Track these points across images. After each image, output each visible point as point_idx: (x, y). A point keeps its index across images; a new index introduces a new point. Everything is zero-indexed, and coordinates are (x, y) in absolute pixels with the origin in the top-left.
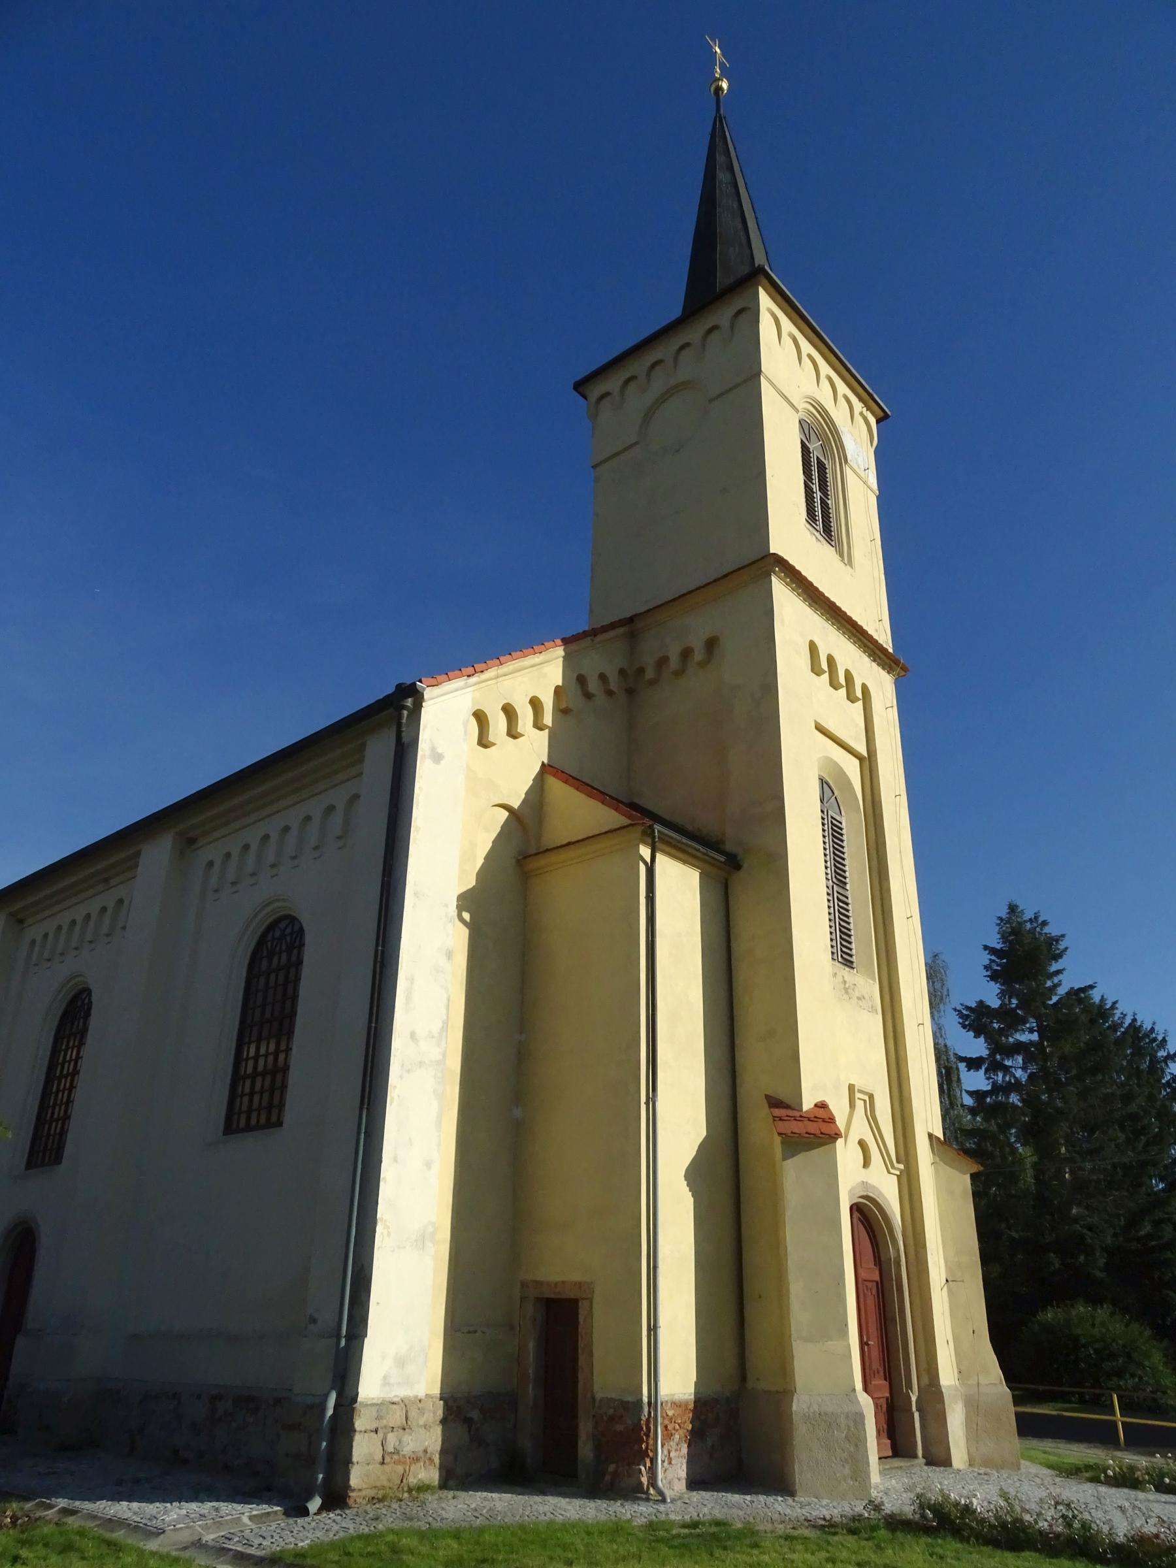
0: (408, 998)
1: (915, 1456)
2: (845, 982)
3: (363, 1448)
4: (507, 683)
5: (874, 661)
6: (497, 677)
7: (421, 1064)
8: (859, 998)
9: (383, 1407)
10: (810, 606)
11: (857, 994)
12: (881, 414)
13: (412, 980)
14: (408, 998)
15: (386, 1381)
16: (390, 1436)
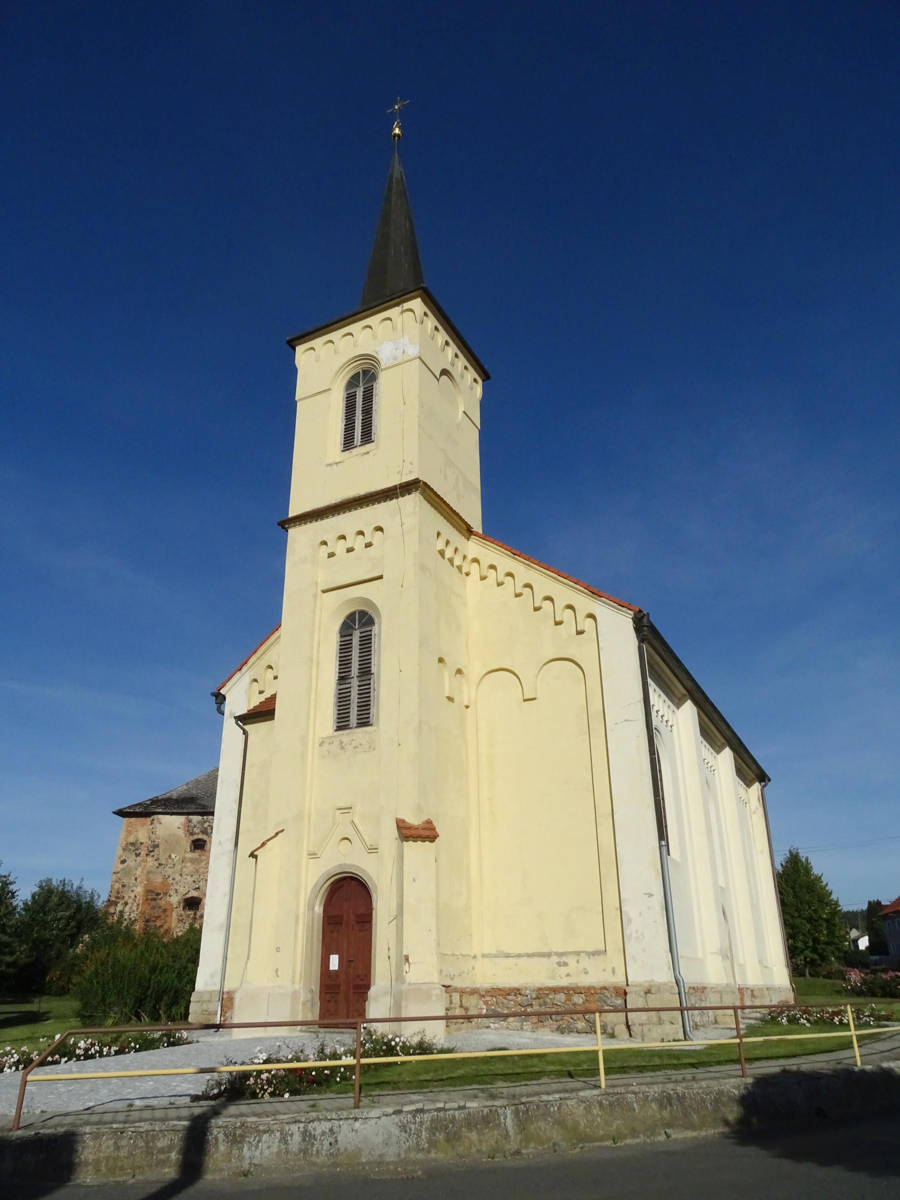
1: (595, 1032)
2: (342, 743)
4: (267, 656)
5: (391, 500)
6: (259, 658)
8: (355, 748)
10: (322, 519)
11: (354, 744)
12: (419, 292)
15: (206, 983)
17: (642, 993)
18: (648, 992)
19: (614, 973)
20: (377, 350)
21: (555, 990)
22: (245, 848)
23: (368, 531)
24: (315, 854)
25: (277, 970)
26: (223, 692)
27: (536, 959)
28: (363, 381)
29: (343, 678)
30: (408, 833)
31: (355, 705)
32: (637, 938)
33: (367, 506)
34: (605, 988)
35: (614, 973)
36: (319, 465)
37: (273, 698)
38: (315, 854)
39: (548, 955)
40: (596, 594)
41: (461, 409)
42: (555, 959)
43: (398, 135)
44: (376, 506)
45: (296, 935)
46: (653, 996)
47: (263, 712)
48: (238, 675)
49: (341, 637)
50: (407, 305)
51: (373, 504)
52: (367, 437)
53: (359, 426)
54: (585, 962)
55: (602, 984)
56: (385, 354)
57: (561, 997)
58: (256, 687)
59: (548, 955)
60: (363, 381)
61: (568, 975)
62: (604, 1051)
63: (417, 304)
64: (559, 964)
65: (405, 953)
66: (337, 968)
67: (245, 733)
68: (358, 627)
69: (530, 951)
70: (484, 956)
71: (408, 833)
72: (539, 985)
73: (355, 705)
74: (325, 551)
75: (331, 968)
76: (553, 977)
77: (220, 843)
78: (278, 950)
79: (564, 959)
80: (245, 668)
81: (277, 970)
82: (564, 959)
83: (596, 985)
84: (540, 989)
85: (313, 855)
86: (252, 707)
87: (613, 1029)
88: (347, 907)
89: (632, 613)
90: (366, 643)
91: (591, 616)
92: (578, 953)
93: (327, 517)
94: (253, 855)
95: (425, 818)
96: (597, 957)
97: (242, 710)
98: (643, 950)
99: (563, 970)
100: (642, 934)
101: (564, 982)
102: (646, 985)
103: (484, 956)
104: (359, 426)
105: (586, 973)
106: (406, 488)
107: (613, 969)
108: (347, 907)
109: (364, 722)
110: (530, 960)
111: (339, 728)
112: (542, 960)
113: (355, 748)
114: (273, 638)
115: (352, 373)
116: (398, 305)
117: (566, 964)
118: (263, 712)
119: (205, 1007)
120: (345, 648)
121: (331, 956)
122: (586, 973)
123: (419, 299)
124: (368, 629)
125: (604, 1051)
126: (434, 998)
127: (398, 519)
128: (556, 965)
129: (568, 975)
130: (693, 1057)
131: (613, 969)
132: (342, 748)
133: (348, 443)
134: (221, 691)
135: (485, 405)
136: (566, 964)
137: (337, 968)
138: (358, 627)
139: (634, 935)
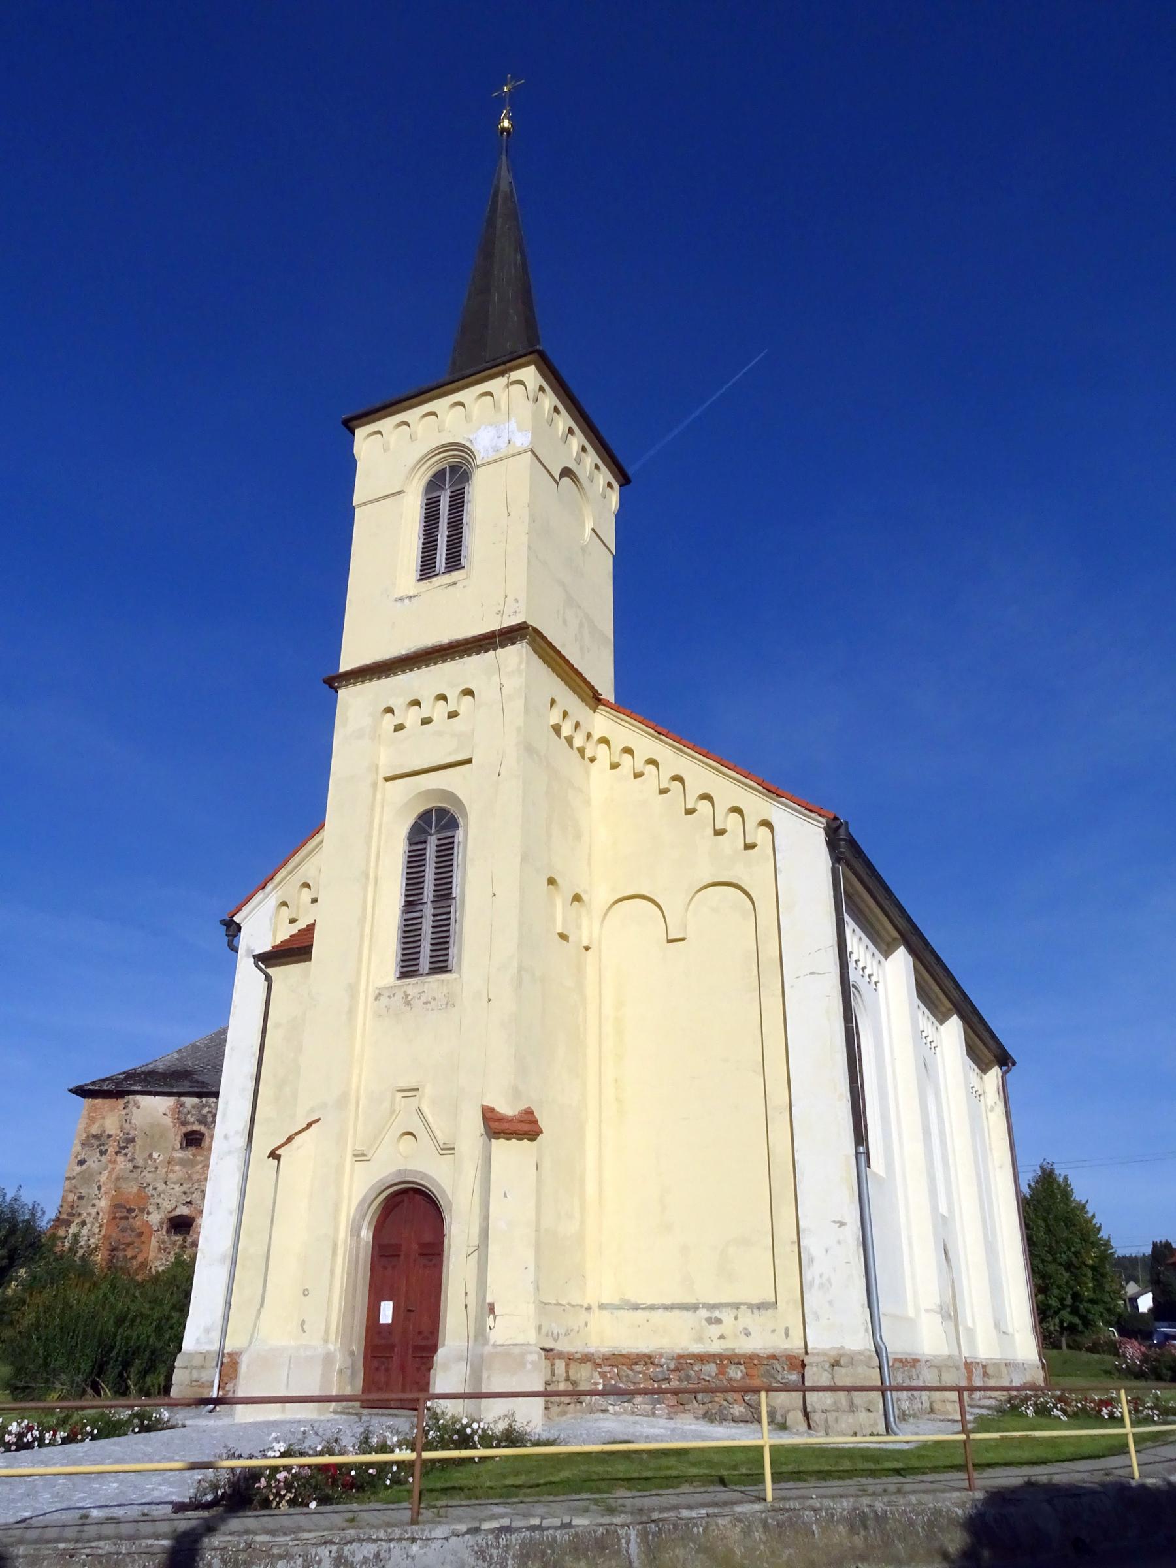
0: (224, 1115)
2: (407, 996)
3: (177, 1376)
4: (303, 869)
5: (487, 651)
6: (291, 872)
7: (230, 1152)
8: (426, 1003)
9: (191, 1355)
10: (387, 677)
11: (424, 999)
13: (227, 1103)
14: (224, 1115)
16: (194, 1372)
17: (827, 1366)
18: (836, 1364)
19: (787, 1335)
20: (471, 437)
21: (702, 1358)
22: (263, 1144)
24: (364, 1155)
25: (303, 1322)
26: (237, 919)
27: (677, 1312)
29: (411, 903)
30: (498, 1127)
31: (427, 941)
32: (821, 1286)
33: (452, 659)
34: (774, 1357)
35: (787, 1335)
36: (384, 596)
37: (311, 928)
38: (364, 1155)
39: (694, 1308)
40: (773, 791)
41: (589, 525)
42: (703, 1313)
43: (507, 130)
44: (465, 659)
46: (844, 1371)
47: (295, 950)
48: (260, 895)
49: (410, 844)
50: (515, 375)
51: (461, 657)
52: (455, 561)
53: (443, 543)
54: (747, 1319)
55: (770, 1351)
56: (483, 443)
57: (712, 1368)
59: (694, 1308)
61: (722, 1337)
62: (773, 1448)
63: (529, 374)
64: (709, 1321)
65: (489, 1300)
66: (390, 1321)
67: (268, 978)
68: (435, 834)
69: (668, 1302)
70: (602, 1307)
71: (498, 1127)
72: (678, 1351)
73: (427, 941)
74: (389, 721)
75: (382, 1321)
76: (700, 1340)
77: (226, 1137)
78: (306, 1293)
79: (717, 1314)
80: (270, 887)
81: (303, 1322)
82: (717, 1314)
83: (761, 1352)
84: (680, 1357)
85: (360, 1156)
87: (784, 1417)
88: (407, 1233)
89: (823, 820)
90: (446, 853)
91: (766, 824)
92: (736, 1306)
93: (395, 674)
95: (523, 1107)
96: (763, 1312)
97: (265, 946)
98: (830, 1303)
99: (715, 1330)
100: (829, 1280)
101: (715, 1347)
102: (833, 1353)
103: (602, 1307)
104: (443, 543)
105: (748, 1334)
107: (787, 1329)
108: (407, 1233)
109: (440, 966)
110: (668, 1314)
111: (403, 975)
112: (685, 1313)
113: (426, 1003)
116: (502, 374)
117: (719, 1321)
118: (295, 950)
119: (195, 1374)
120: (415, 861)
121: (382, 1304)
122: (748, 1334)
123: (533, 367)
124: (449, 834)
125: (773, 1448)
126: (529, 1366)
127: (496, 678)
128: (704, 1323)
129: (722, 1337)
131: (787, 1329)
132: (408, 1003)
133: (427, 569)
134: (235, 918)
135: (623, 520)
136: (719, 1321)
137: (390, 1321)
138: (435, 834)
139: (817, 1281)
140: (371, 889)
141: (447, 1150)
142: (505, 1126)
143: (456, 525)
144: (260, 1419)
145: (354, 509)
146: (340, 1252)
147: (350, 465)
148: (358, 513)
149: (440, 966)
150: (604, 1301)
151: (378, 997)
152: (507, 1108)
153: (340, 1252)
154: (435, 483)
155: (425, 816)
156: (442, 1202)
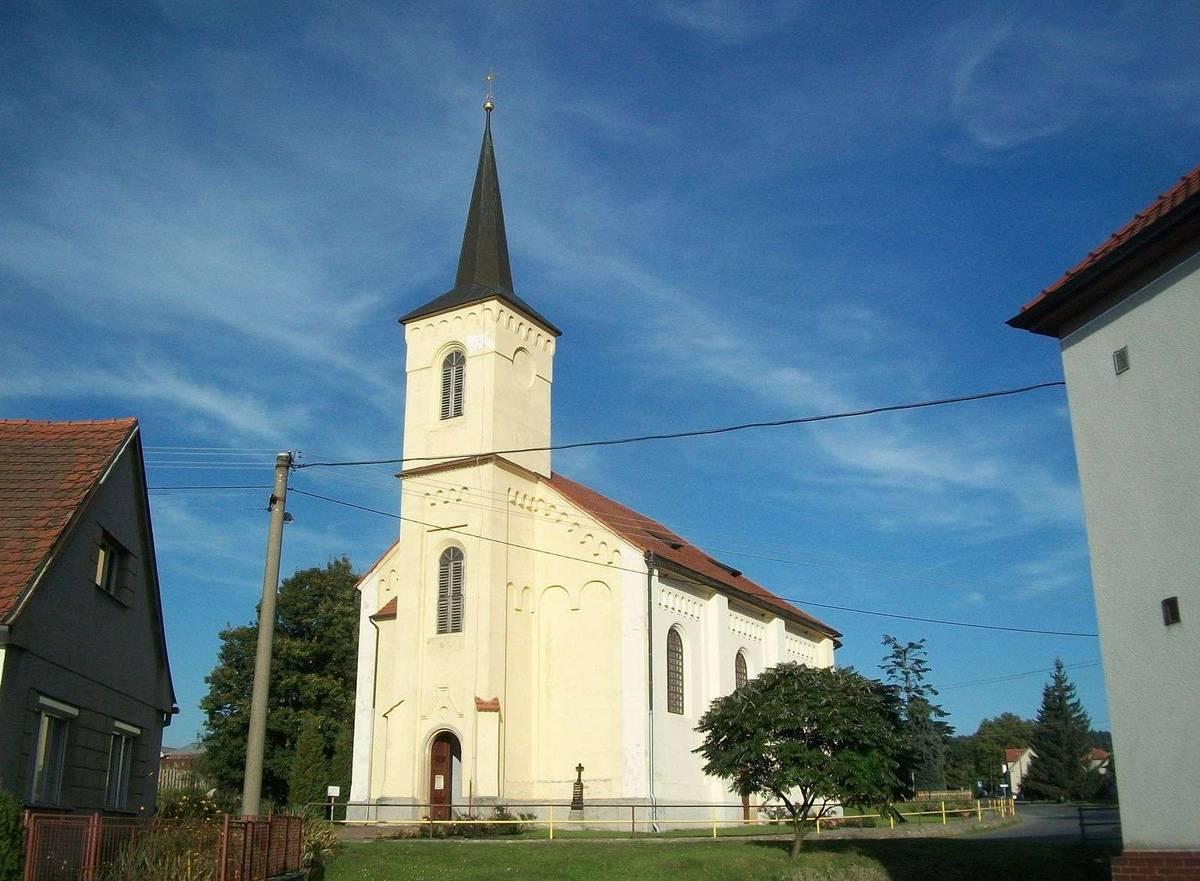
4: (391, 562)
15: (358, 797)
22: (381, 709)
23: (458, 489)
28: (455, 361)
29: (442, 597)
30: (482, 706)
31: (450, 619)
36: (424, 432)
37: (394, 601)
41: (534, 373)
45: (414, 767)
47: (388, 613)
49: (441, 565)
50: (487, 304)
52: (458, 413)
53: (452, 403)
58: (384, 586)
60: (455, 361)
66: (338, 788)
67: (376, 627)
68: (452, 559)
70: (539, 782)
71: (482, 706)
73: (450, 619)
74: (428, 501)
86: (381, 607)
88: (446, 747)
90: (458, 571)
94: (384, 716)
95: (494, 697)
97: (374, 612)
103: (539, 782)
104: (452, 403)
106: (484, 459)
108: (446, 747)
109: (457, 629)
111: (440, 632)
114: (394, 549)
115: (448, 354)
118: (388, 613)
120: (443, 575)
130: (59, 715)
133: (445, 415)
135: (557, 359)
138: (452, 559)
140: (421, 617)
141: (461, 715)
142: (484, 706)
143: (459, 389)
144: (56, 707)
145: (406, 374)
146: (417, 758)
147: (403, 347)
148: (409, 374)
149: (457, 629)
150: (541, 779)
151: (428, 643)
152: (486, 698)
153: (417, 758)
154: (447, 363)
155: (448, 551)
156: (459, 738)
